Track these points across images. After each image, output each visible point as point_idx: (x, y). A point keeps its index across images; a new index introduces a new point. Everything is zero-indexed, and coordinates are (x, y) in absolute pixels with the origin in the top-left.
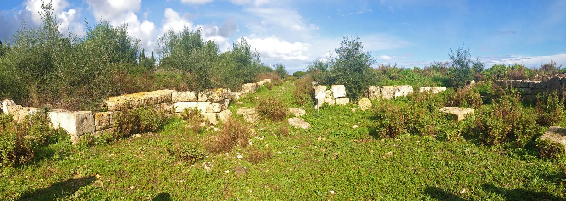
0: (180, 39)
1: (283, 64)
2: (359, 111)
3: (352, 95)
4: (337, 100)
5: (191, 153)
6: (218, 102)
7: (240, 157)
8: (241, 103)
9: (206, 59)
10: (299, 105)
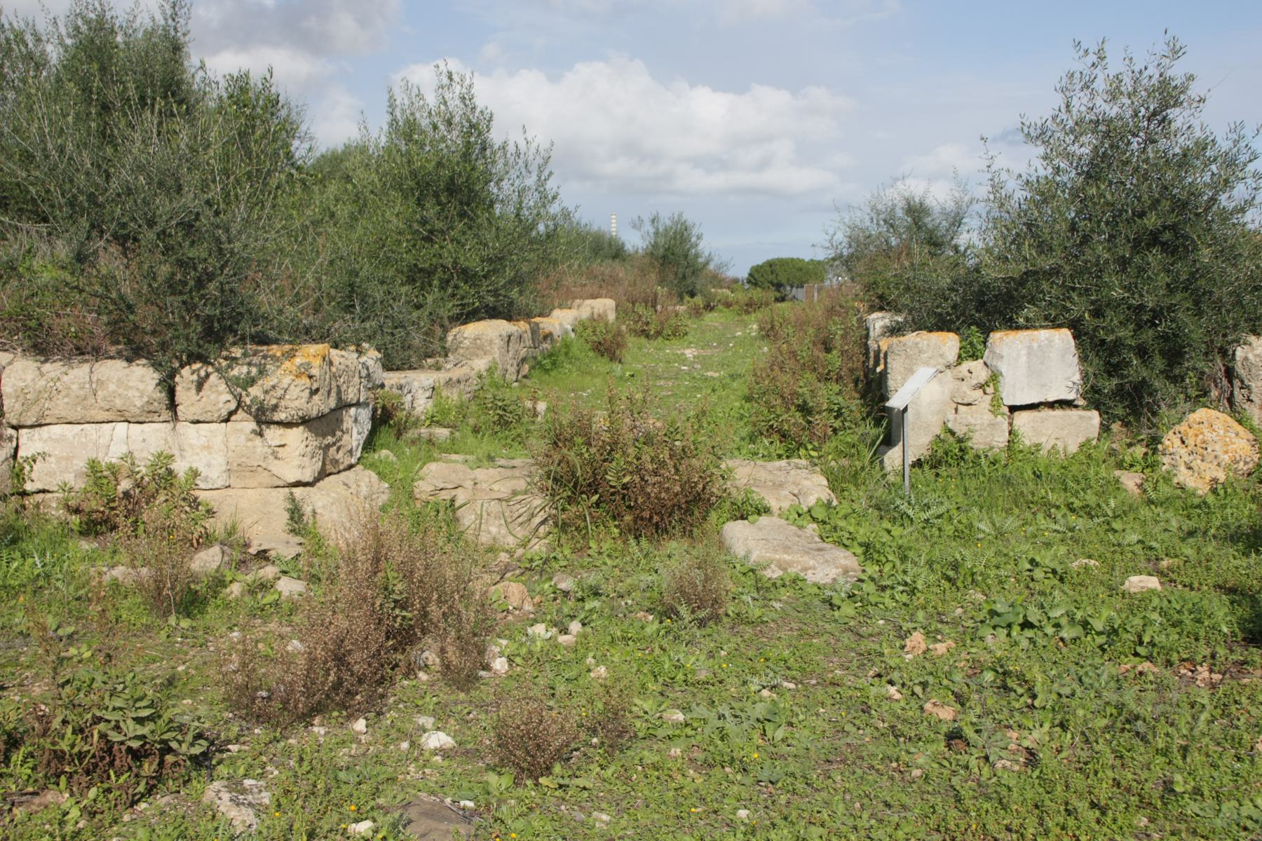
0: (54, 53)
1: (689, 217)
2: (1165, 490)
3: (1119, 393)
4: (1022, 418)
5: (131, 728)
6: (305, 421)
7: (437, 740)
8: (442, 433)
9: (226, 173)
10: (790, 444)
